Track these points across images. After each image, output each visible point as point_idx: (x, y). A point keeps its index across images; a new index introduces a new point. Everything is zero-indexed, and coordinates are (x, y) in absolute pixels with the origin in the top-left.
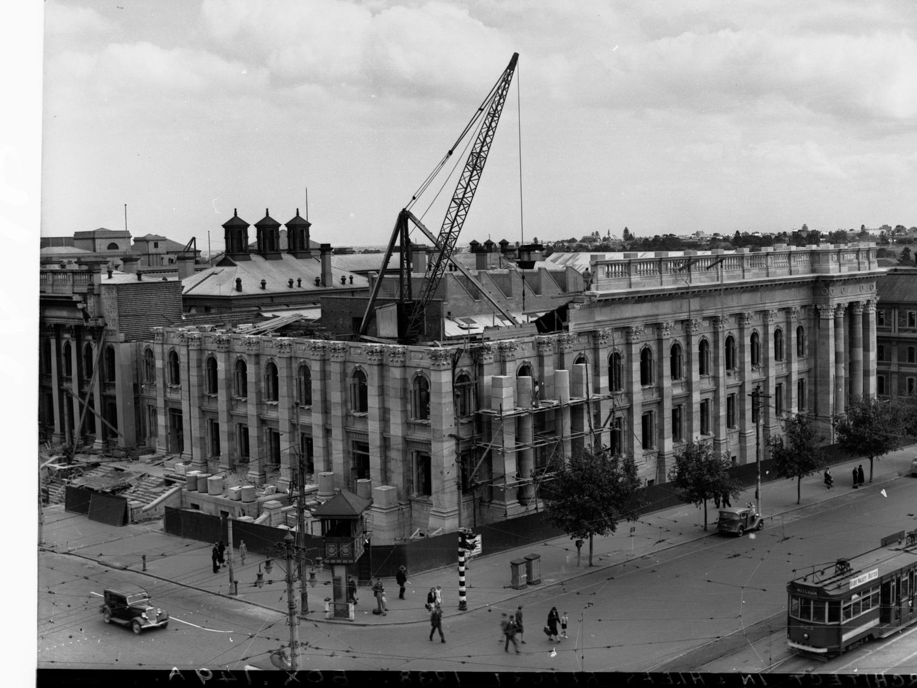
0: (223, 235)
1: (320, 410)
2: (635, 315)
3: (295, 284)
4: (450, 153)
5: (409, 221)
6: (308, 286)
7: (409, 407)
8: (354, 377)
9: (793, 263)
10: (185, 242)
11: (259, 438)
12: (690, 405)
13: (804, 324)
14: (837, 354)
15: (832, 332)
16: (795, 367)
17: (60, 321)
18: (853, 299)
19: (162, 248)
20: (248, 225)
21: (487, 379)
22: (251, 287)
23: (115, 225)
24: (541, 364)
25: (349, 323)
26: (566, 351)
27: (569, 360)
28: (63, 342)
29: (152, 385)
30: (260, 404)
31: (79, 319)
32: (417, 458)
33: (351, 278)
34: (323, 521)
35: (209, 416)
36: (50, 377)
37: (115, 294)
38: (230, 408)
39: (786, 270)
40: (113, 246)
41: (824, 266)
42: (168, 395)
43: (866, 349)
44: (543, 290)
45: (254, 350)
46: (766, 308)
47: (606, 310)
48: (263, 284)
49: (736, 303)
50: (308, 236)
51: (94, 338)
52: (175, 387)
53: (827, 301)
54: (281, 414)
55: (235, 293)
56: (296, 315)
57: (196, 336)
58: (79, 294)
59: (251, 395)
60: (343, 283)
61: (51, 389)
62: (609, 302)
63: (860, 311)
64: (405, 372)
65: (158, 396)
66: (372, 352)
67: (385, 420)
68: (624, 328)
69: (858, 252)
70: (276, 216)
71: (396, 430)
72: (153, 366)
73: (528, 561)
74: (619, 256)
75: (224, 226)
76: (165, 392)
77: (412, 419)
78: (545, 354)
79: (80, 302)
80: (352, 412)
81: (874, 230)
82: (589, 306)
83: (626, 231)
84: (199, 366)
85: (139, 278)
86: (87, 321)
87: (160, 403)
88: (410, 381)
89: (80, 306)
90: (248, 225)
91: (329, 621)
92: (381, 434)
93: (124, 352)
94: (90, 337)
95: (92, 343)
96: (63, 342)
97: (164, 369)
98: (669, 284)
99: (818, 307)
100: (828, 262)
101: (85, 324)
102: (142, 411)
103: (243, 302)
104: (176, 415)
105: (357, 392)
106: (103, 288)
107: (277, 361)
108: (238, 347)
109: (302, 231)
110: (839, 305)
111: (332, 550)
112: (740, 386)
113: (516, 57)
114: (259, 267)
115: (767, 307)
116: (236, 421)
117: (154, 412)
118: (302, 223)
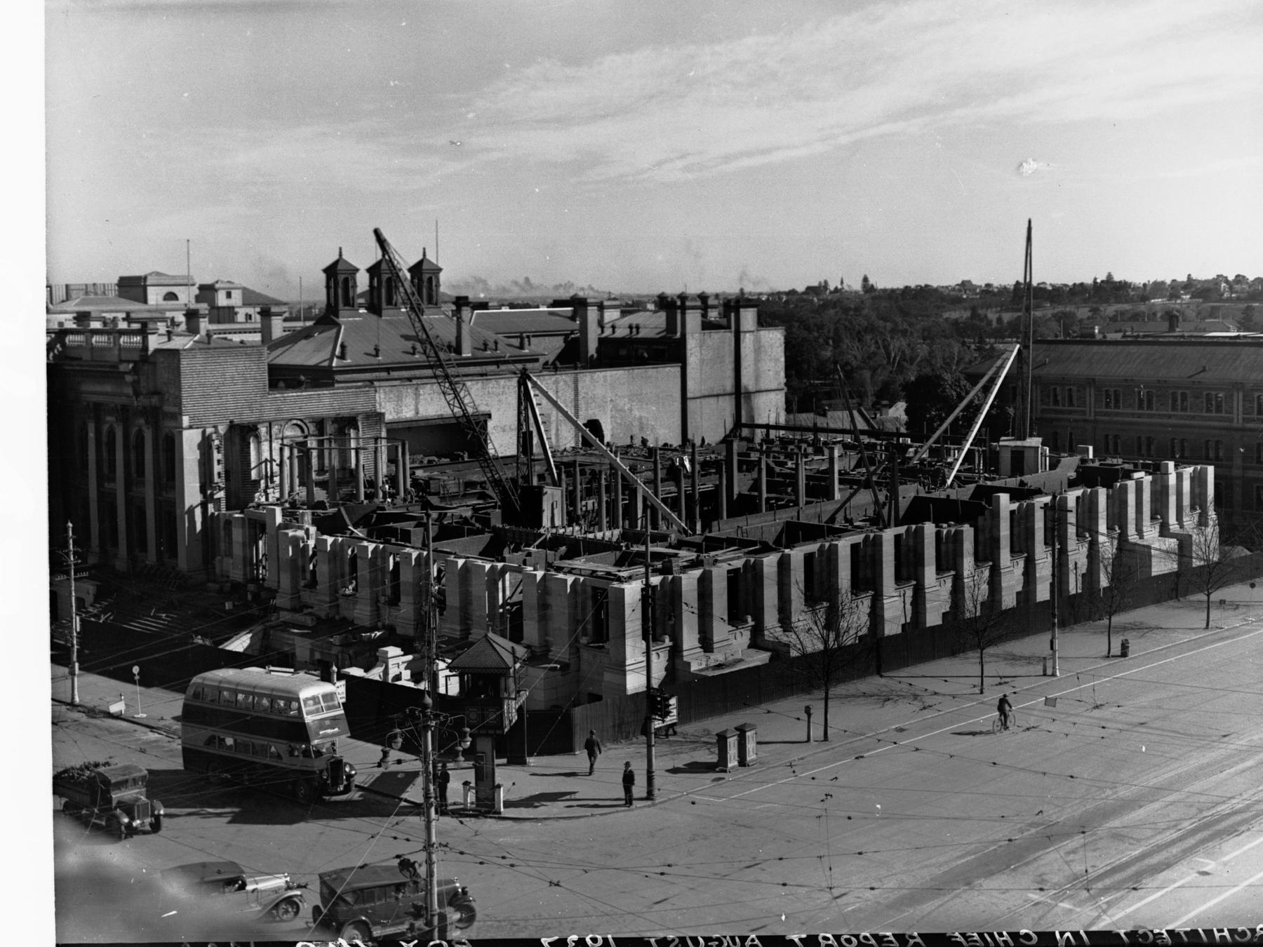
0: (324, 283)
17: (101, 399)
20: (357, 270)
28: (105, 428)
31: (128, 396)
36: (143, 483)
40: (171, 296)
50: (438, 285)
51: (147, 422)
70: (351, 258)
73: (741, 732)
83: (865, 279)
90: (357, 270)
94: (142, 421)
95: (144, 428)
96: (105, 428)
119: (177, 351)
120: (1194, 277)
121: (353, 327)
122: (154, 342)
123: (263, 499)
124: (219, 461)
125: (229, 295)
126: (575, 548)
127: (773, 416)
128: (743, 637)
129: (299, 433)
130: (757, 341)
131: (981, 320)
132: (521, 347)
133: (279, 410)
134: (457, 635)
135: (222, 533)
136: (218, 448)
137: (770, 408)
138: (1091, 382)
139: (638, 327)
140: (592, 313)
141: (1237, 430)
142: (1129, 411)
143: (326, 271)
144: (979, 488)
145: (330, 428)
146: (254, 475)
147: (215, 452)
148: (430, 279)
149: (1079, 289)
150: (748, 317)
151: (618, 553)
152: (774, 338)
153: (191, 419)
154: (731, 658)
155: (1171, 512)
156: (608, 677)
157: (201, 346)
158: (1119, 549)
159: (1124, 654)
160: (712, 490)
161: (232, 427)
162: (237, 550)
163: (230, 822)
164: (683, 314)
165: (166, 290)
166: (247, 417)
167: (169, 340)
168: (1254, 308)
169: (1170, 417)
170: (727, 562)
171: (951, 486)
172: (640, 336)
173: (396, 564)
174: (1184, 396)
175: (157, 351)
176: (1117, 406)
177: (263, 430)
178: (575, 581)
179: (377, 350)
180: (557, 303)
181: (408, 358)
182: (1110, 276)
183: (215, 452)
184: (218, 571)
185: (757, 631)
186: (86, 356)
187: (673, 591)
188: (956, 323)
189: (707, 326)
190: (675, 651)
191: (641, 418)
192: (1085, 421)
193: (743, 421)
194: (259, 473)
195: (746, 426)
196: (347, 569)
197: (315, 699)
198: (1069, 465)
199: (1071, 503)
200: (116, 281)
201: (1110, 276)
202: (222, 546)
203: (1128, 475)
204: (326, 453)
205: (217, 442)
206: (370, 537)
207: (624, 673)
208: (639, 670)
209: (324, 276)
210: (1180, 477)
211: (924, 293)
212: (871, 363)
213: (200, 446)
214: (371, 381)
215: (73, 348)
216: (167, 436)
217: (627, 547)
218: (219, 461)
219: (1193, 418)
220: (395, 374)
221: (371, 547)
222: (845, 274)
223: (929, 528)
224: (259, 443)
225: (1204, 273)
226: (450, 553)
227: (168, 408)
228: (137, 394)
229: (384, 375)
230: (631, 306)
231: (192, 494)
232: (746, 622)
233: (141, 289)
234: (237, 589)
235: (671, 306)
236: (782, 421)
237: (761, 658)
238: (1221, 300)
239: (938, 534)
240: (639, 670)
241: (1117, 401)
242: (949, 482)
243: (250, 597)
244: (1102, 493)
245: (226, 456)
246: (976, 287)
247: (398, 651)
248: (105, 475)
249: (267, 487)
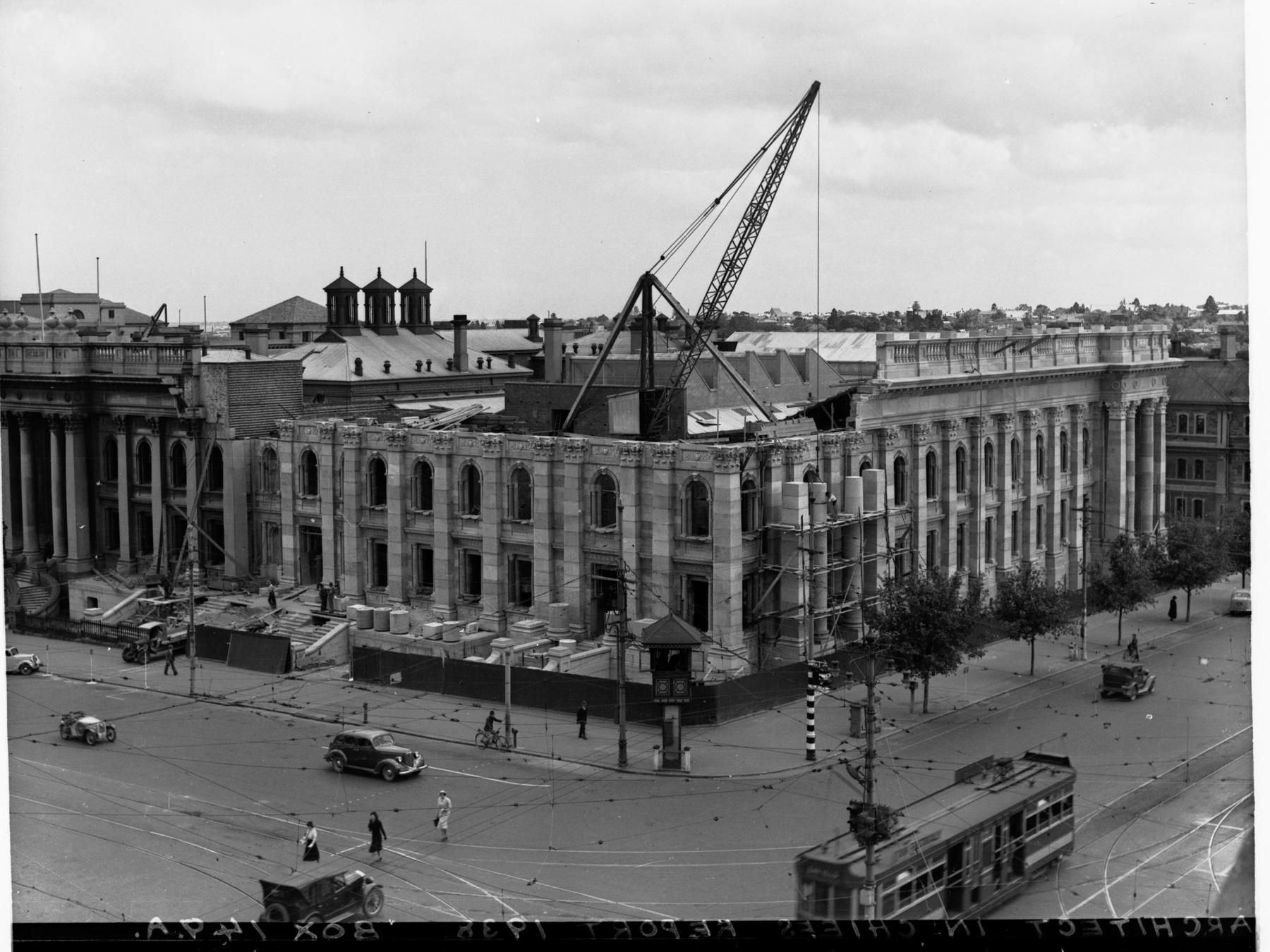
1: (546, 524)
2: (923, 409)
3: (425, 366)
4: (718, 201)
5: (653, 288)
6: (439, 370)
7: (678, 520)
8: (596, 483)
9: (1081, 350)
10: (150, 312)
11: (450, 563)
12: (974, 524)
13: (1089, 425)
14: (1128, 463)
15: (1123, 436)
16: (1081, 479)
17: (134, 411)
18: (1145, 395)
19: (119, 318)
21: (776, 485)
22: (372, 371)
23: (79, 285)
24: (827, 469)
25: (546, 416)
26: (853, 453)
27: (855, 465)
28: (136, 440)
29: (274, 496)
30: (452, 518)
32: (687, 582)
33: (489, 361)
34: (652, 652)
35: (370, 535)
36: (116, 486)
37: (223, 376)
38: (406, 524)
39: (1073, 358)
41: (1116, 354)
42: (299, 509)
43: (1157, 460)
44: (782, 379)
45: (445, 449)
46: (1054, 405)
47: (894, 403)
48: (387, 366)
49: (1025, 399)
52: (310, 497)
53: (1118, 396)
54: (486, 530)
55: (354, 378)
56: (475, 406)
57: (356, 431)
58: (174, 375)
59: (440, 506)
60: (419, 370)
61: (116, 501)
62: (900, 392)
63: (1151, 411)
64: (674, 476)
65: (286, 508)
66: (628, 451)
67: (643, 534)
68: (910, 426)
69: (1150, 336)
71: (661, 548)
72: (276, 471)
74: (903, 337)
75: (326, 289)
76: (294, 504)
77: (683, 536)
78: (833, 456)
79: (174, 386)
80: (593, 527)
82: (878, 398)
84: (358, 471)
85: (248, 357)
87: (287, 519)
88: (680, 487)
89: (173, 391)
91: (658, 773)
92: (638, 554)
93: (235, 454)
96: (136, 440)
97: (293, 474)
98: (957, 372)
99: (1107, 404)
100: (1120, 348)
101: (179, 415)
102: (260, 533)
103: (365, 389)
104: (311, 538)
105: (599, 501)
106: (204, 368)
107: (480, 465)
108: (417, 444)
109: (347, 299)
110: (1132, 402)
112: (1024, 503)
113: (816, 87)
114: (372, 345)
115: (1054, 403)
116: (412, 540)
117: (276, 531)
118: (385, 287)
182: (554, 315)
209: (325, 295)
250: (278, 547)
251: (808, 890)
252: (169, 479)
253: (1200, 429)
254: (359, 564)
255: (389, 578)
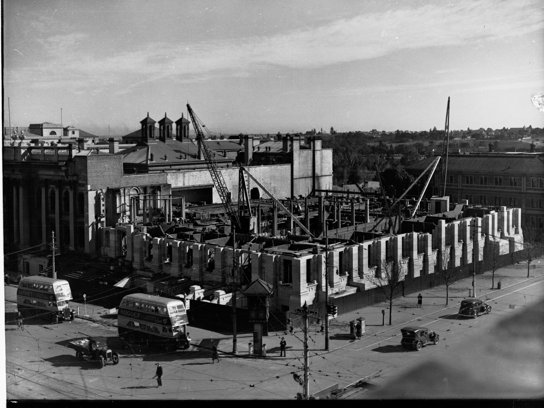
17: (49, 177)
28: (50, 190)
31: (62, 176)
36: (69, 215)
40: (53, 133)
51: (71, 188)
75: (141, 122)
81: (304, 133)
83: (332, 129)
86: (67, 177)
94: (68, 187)
95: (69, 191)
96: (50, 190)
111: (253, 315)
119: (86, 156)
120: (470, 129)
121: (153, 146)
122: (75, 153)
123: (122, 222)
124: (103, 205)
125: (73, 133)
126: (270, 243)
127: (328, 186)
128: (344, 281)
129: (136, 193)
130: (322, 154)
131: (384, 146)
132: (225, 156)
133: (127, 183)
134: (220, 280)
135: (104, 236)
136: (103, 199)
137: (327, 183)
138: (460, 173)
139: (270, 148)
140: (250, 141)
141: (524, 193)
142: (477, 185)
143: (141, 122)
144: (427, 217)
145: (149, 191)
146: (118, 211)
147: (102, 201)
148: (168, 127)
149: (423, 134)
150: (318, 144)
151: (289, 245)
152: (328, 153)
153: (91, 186)
154: (341, 290)
155: (506, 229)
156: (292, 298)
157: (94, 154)
158: (486, 243)
159: (499, 288)
160: (317, 218)
161: (108, 190)
162: (112, 243)
163: (52, 365)
164: (292, 142)
165: (50, 130)
166: (115, 186)
167: (79, 152)
168: (498, 142)
169: (494, 188)
170: (338, 250)
171: (414, 217)
172: (271, 152)
173: (190, 250)
174: (500, 180)
175: (76, 156)
176: (471, 183)
177: (122, 191)
178: (276, 257)
179: (166, 157)
180: (232, 137)
181: (178, 160)
182: (435, 128)
183: (102, 201)
184: (102, 253)
185: (350, 278)
186: (42, 159)
187: (318, 261)
188: (373, 148)
189: (302, 148)
190: (319, 287)
191: (274, 187)
192: (458, 189)
193: (316, 189)
194: (120, 209)
195: (317, 191)
196: (166, 252)
197: (174, 308)
198: (459, 209)
199: (468, 223)
200: (28, 126)
201: (435, 128)
202: (104, 242)
203: (488, 212)
204: (148, 202)
205: (102, 197)
206: (178, 238)
207: (300, 296)
208: (307, 295)
209: (141, 124)
210: (508, 213)
211: (358, 135)
212: (343, 164)
213: (95, 198)
214: (163, 171)
215: (34, 155)
216: (80, 194)
217: (293, 242)
218: (103, 205)
219: (504, 188)
220: (173, 167)
221: (179, 242)
222: (364, 125)
223: (415, 235)
224: (120, 197)
225: (475, 127)
226: (216, 245)
227: (81, 182)
228: (67, 176)
229: (169, 167)
230: (264, 139)
231: (92, 219)
232: (345, 274)
233: (40, 130)
234: (112, 261)
235: (286, 139)
236: (331, 189)
237: (352, 291)
238: (484, 139)
239: (418, 236)
240: (307, 295)
241: (471, 181)
242: (413, 215)
243: (120, 264)
244: (480, 220)
245: (106, 203)
246: (379, 132)
247: (199, 287)
248: (51, 210)
249: (123, 216)
250: (108, 241)
251: (14, 290)
252: (63, 208)
253: (533, 186)
254: (141, 248)
255: (216, 267)
